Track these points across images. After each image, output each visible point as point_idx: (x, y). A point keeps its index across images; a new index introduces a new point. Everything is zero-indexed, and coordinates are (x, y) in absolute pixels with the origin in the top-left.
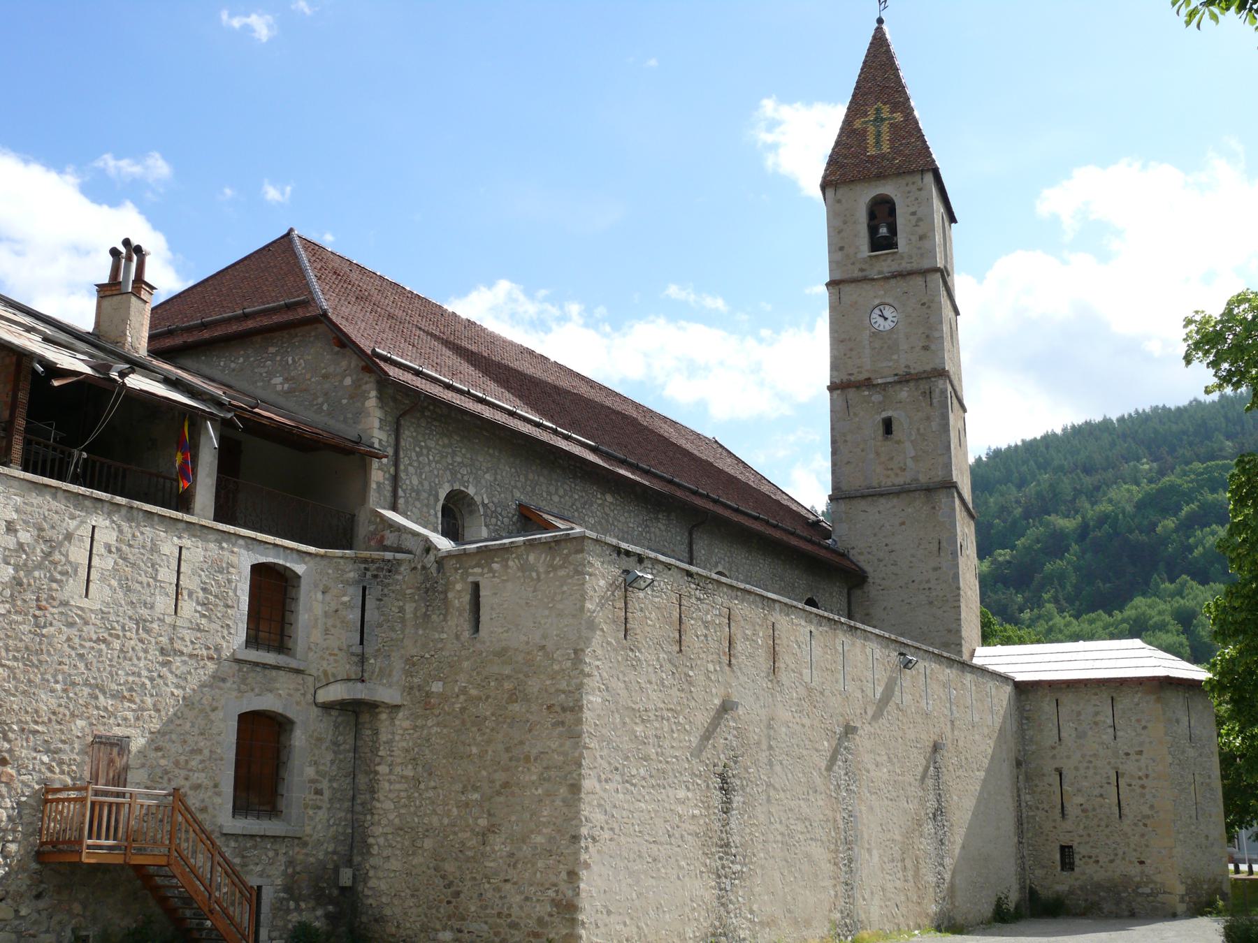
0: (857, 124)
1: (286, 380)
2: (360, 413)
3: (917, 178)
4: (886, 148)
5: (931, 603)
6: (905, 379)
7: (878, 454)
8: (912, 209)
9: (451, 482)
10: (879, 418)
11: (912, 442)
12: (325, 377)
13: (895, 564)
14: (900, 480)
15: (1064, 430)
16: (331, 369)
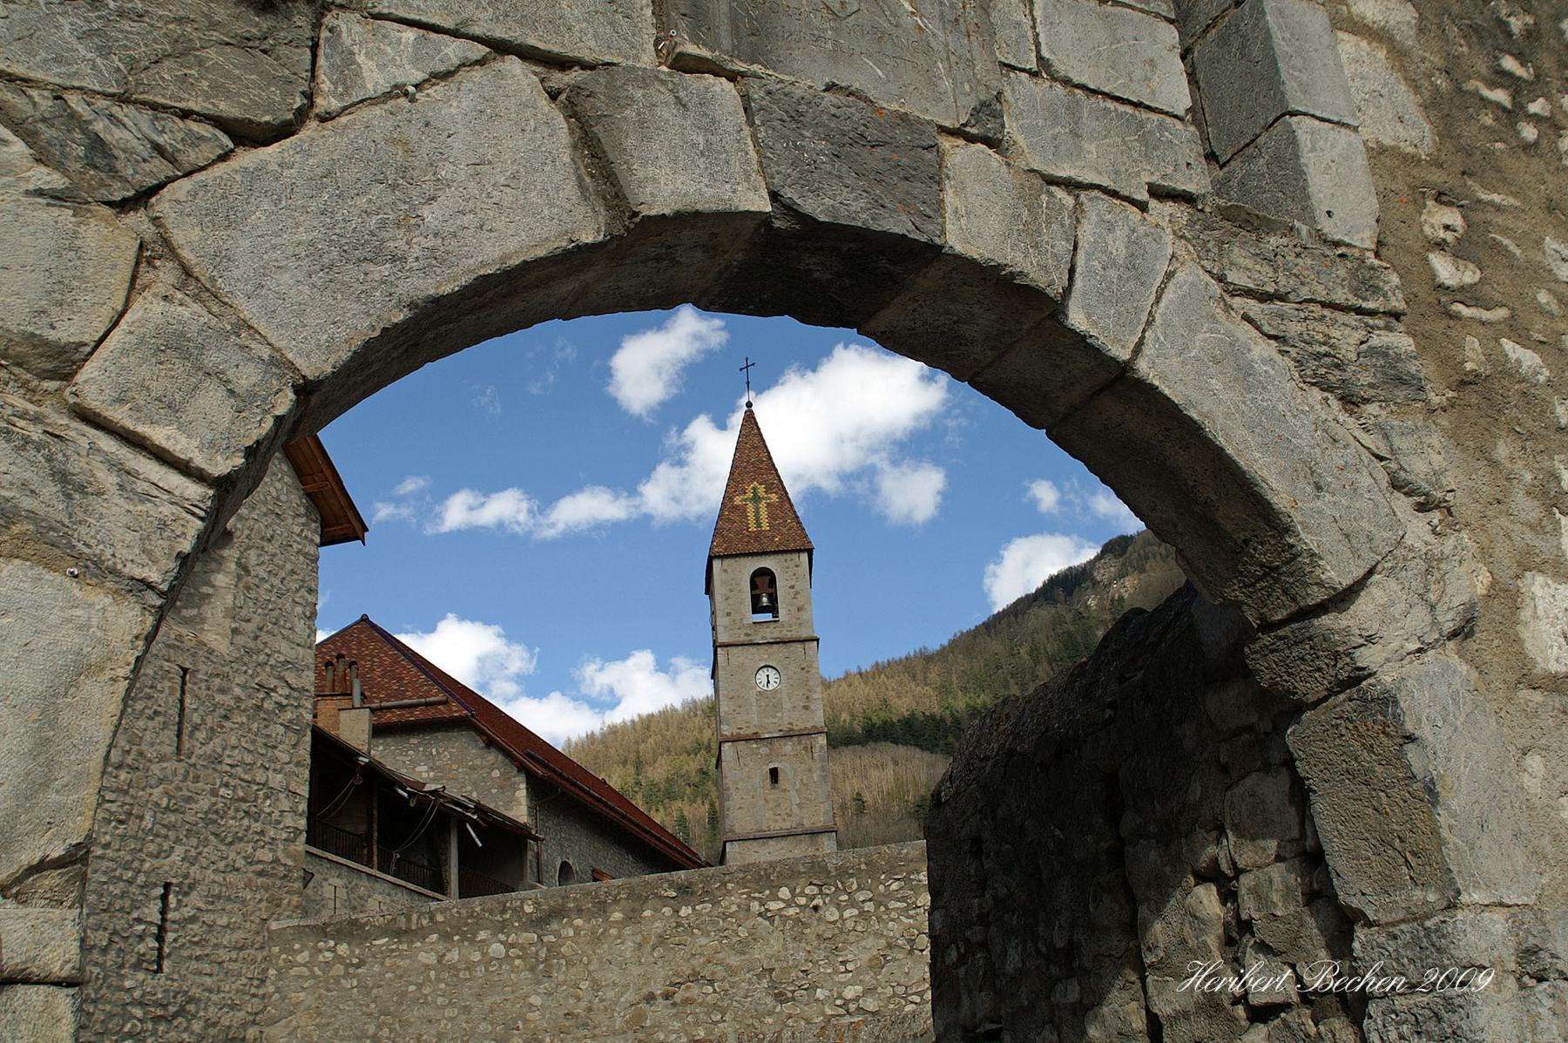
0: (738, 500)
1: (431, 769)
2: (511, 802)
3: (795, 556)
4: (765, 526)
6: (788, 736)
7: (767, 801)
8: (792, 583)
9: (561, 855)
10: (767, 769)
11: (797, 791)
12: (473, 768)
14: (787, 825)
15: (684, 704)
16: (478, 762)
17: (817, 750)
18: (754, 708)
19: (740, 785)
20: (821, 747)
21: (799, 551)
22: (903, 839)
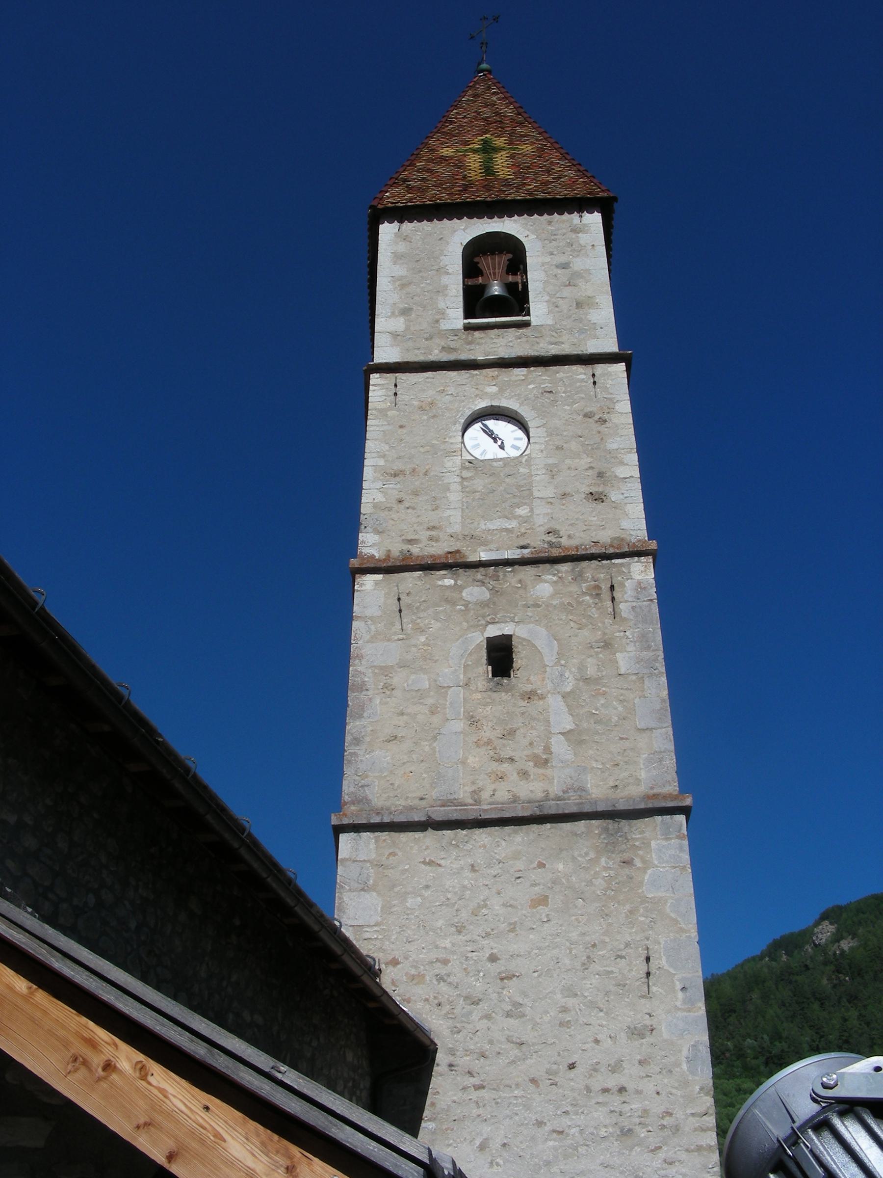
5: (626, 1133)
7: (473, 721)
8: (563, 259)
10: (478, 640)
13: (515, 1012)
17: (627, 594)
18: (454, 497)
19: (397, 679)
20: (640, 587)
21: (580, 205)
22: (355, 616)
